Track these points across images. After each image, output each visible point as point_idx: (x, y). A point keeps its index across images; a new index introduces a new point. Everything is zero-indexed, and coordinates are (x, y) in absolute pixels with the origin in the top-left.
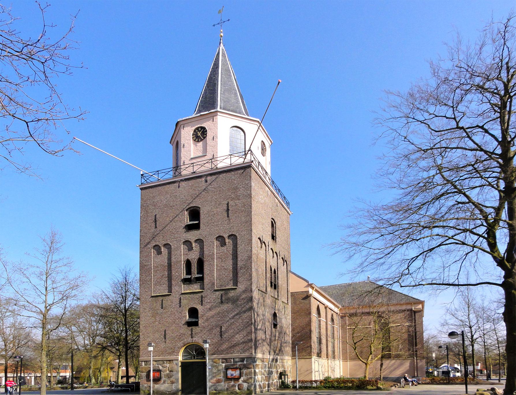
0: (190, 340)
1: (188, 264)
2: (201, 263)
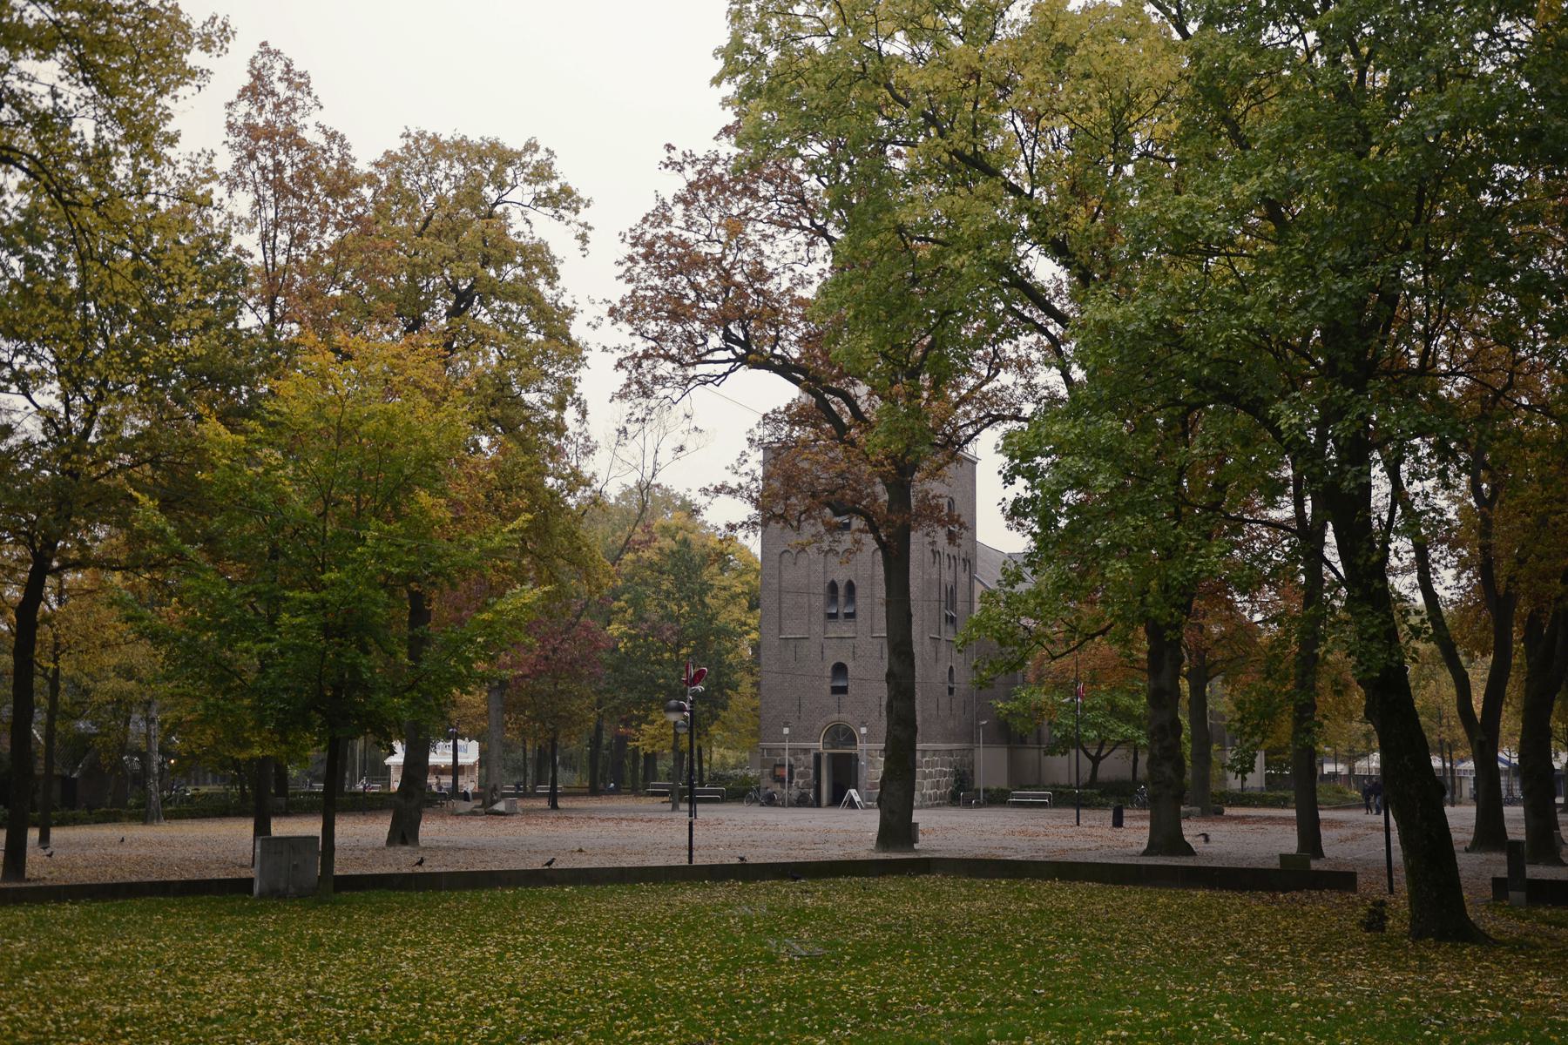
0: (835, 716)
1: (833, 587)
2: (851, 587)
